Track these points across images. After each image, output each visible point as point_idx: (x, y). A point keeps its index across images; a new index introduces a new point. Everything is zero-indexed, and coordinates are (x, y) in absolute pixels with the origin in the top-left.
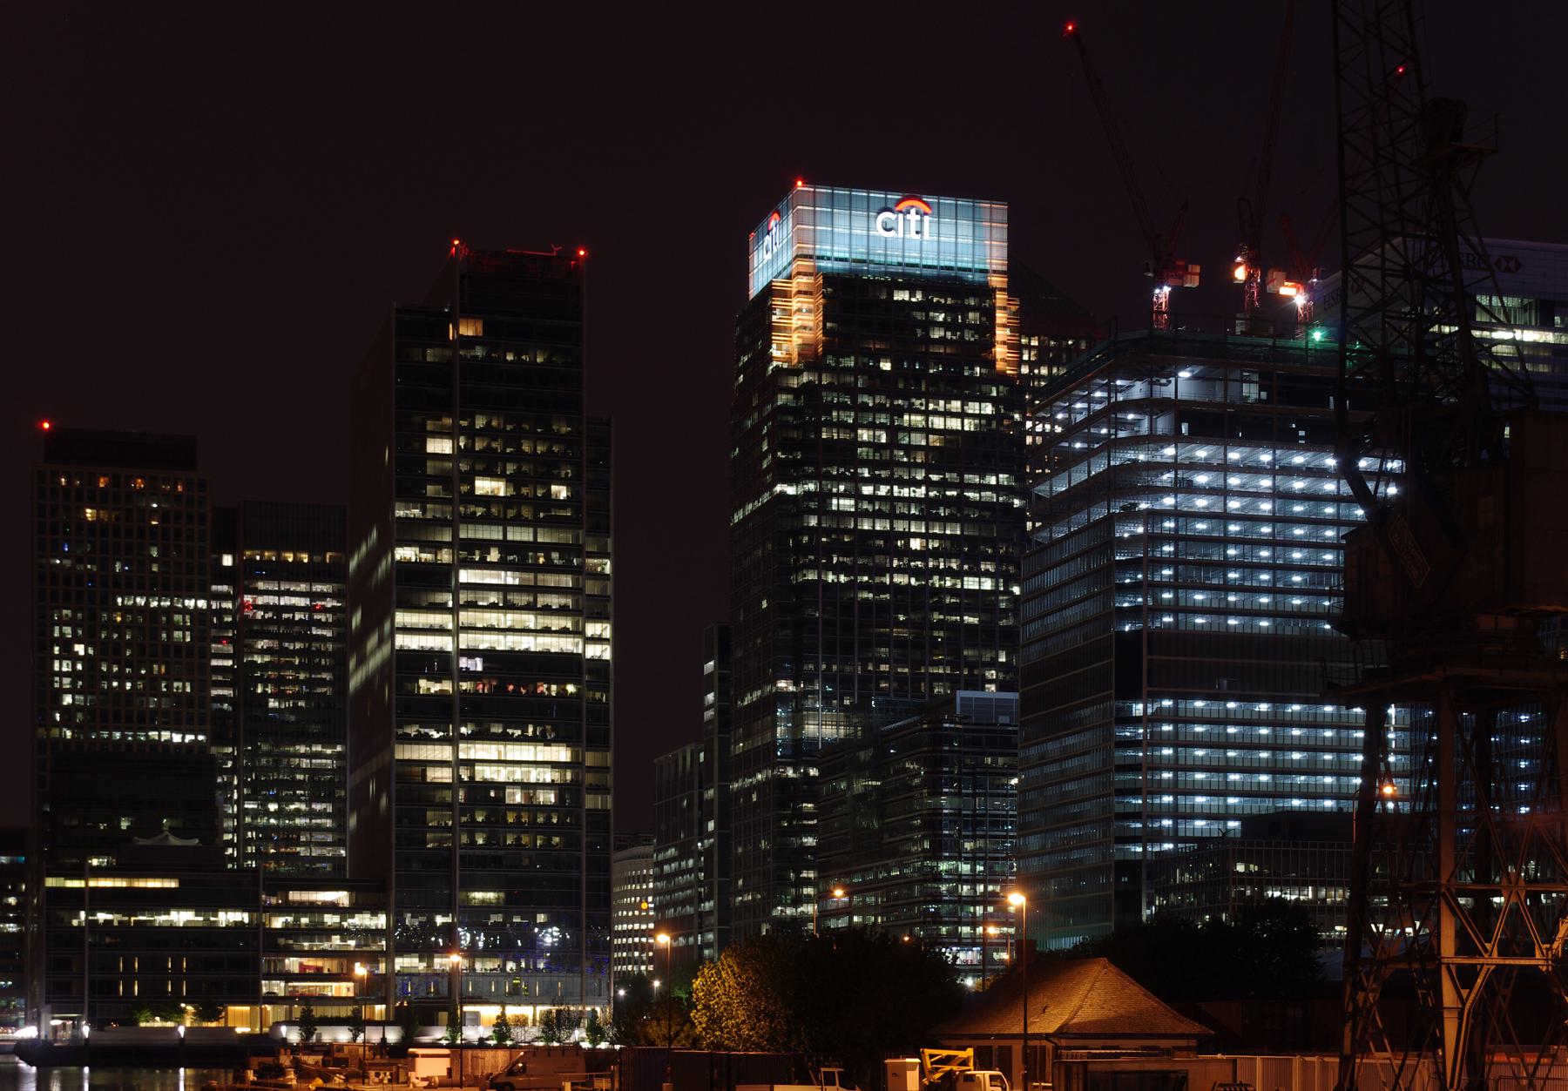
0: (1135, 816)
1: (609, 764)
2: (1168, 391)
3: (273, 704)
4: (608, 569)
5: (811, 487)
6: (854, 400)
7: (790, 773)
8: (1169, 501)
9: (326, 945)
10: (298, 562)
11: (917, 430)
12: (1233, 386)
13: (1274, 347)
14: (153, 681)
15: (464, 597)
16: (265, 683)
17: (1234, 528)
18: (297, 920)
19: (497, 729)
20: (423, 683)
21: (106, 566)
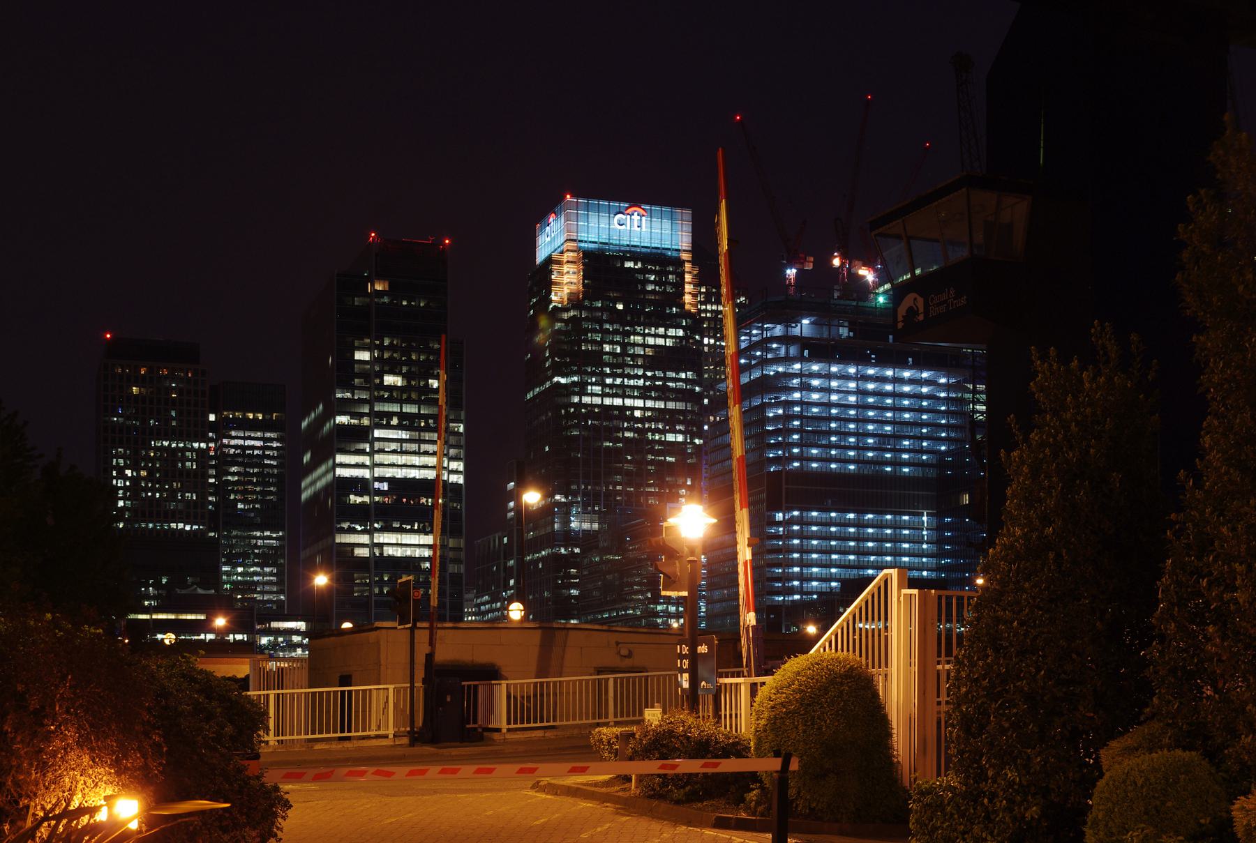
0: (778, 579)
1: (462, 546)
2: (796, 331)
3: (240, 506)
4: (461, 429)
5: (576, 379)
6: (601, 326)
7: (563, 551)
8: (797, 395)
9: (293, 654)
10: (255, 419)
11: (639, 345)
12: (833, 329)
13: (857, 306)
14: (173, 493)
15: (377, 445)
16: (236, 493)
17: (834, 411)
18: (276, 639)
19: (396, 525)
20: (352, 497)
21: (145, 422)
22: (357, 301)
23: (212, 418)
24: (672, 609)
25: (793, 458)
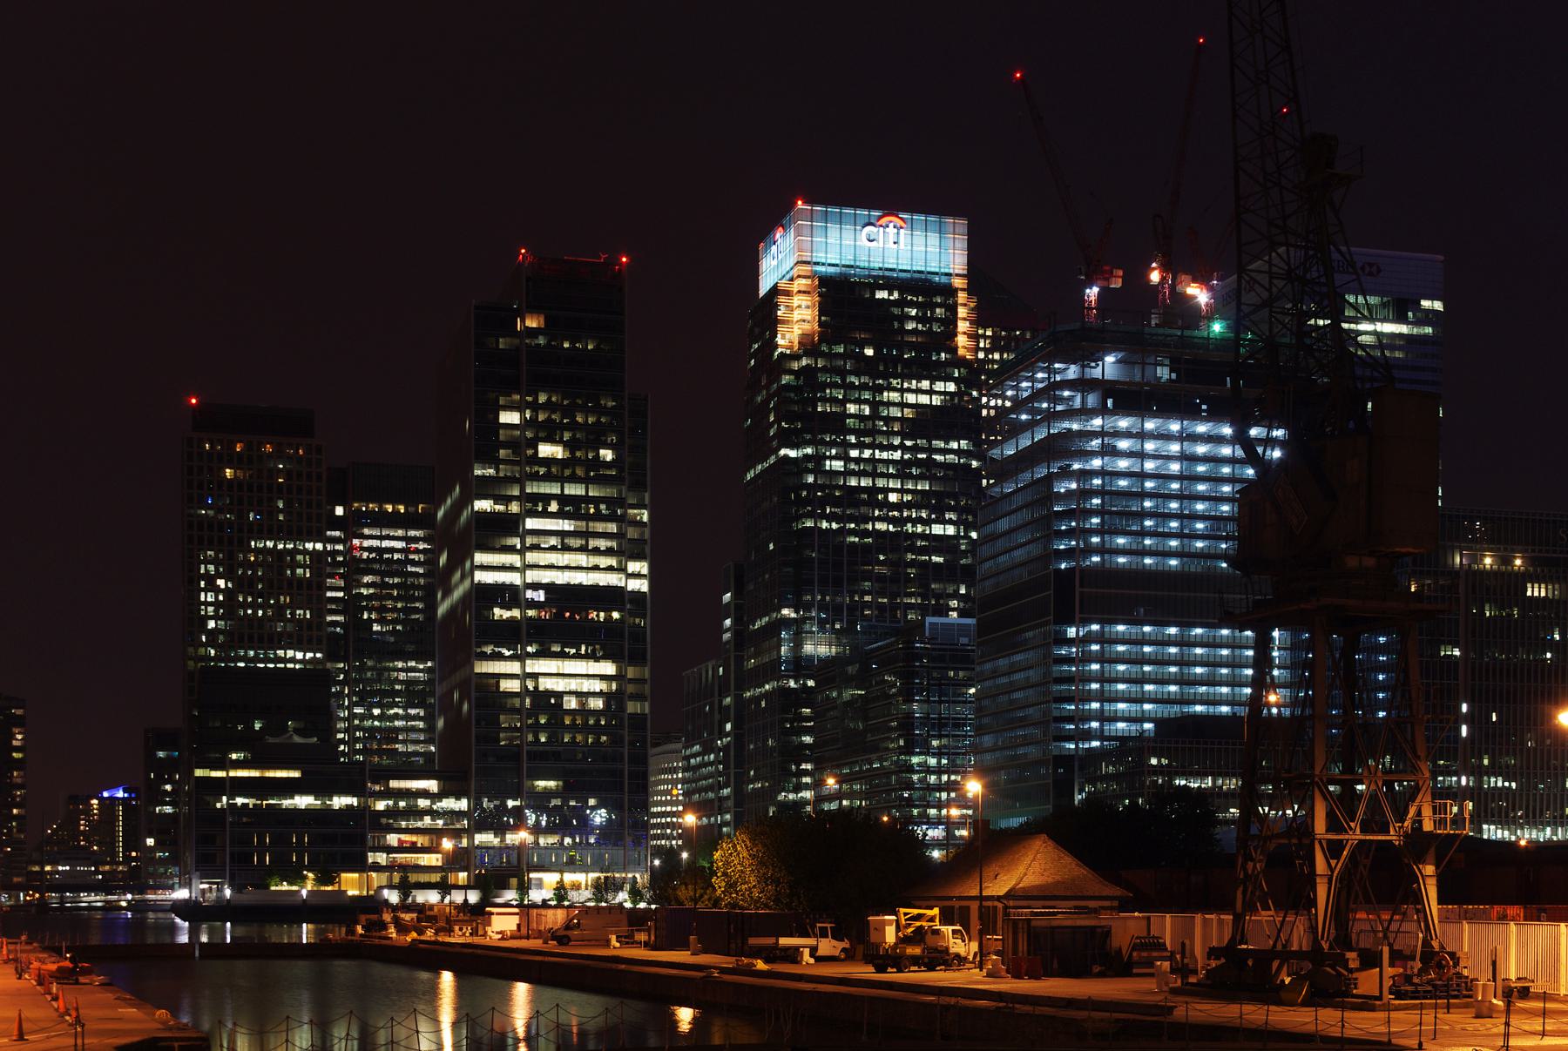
1: (647, 676)
2: (1096, 373)
3: (376, 627)
4: (645, 518)
5: (809, 451)
6: (844, 380)
7: (792, 684)
8: (1097, 463)
9: (419, 824)
10: (396, 512)
13: (1182, 336)
14: (279, 609)
18: (396, 804)
19: (556, 648)
20: (497, 611)
21: (242, 516)
22: (503, 343)
23: (339, 511)
24: (933, 761)
25: (1090, 550)
